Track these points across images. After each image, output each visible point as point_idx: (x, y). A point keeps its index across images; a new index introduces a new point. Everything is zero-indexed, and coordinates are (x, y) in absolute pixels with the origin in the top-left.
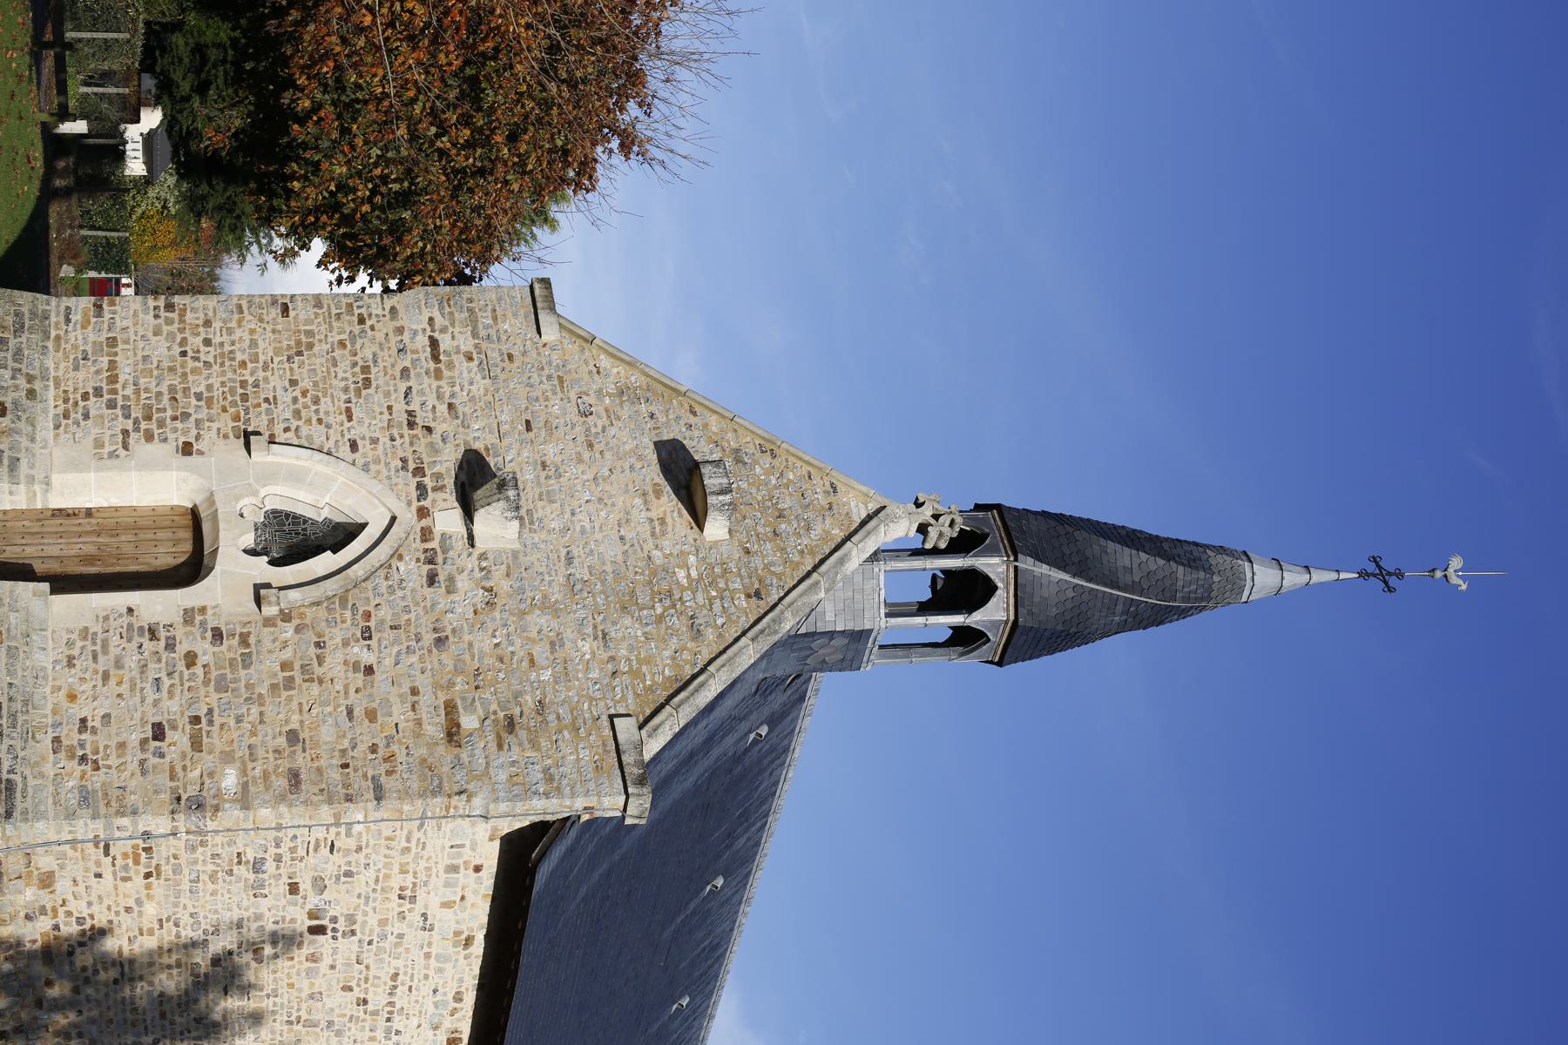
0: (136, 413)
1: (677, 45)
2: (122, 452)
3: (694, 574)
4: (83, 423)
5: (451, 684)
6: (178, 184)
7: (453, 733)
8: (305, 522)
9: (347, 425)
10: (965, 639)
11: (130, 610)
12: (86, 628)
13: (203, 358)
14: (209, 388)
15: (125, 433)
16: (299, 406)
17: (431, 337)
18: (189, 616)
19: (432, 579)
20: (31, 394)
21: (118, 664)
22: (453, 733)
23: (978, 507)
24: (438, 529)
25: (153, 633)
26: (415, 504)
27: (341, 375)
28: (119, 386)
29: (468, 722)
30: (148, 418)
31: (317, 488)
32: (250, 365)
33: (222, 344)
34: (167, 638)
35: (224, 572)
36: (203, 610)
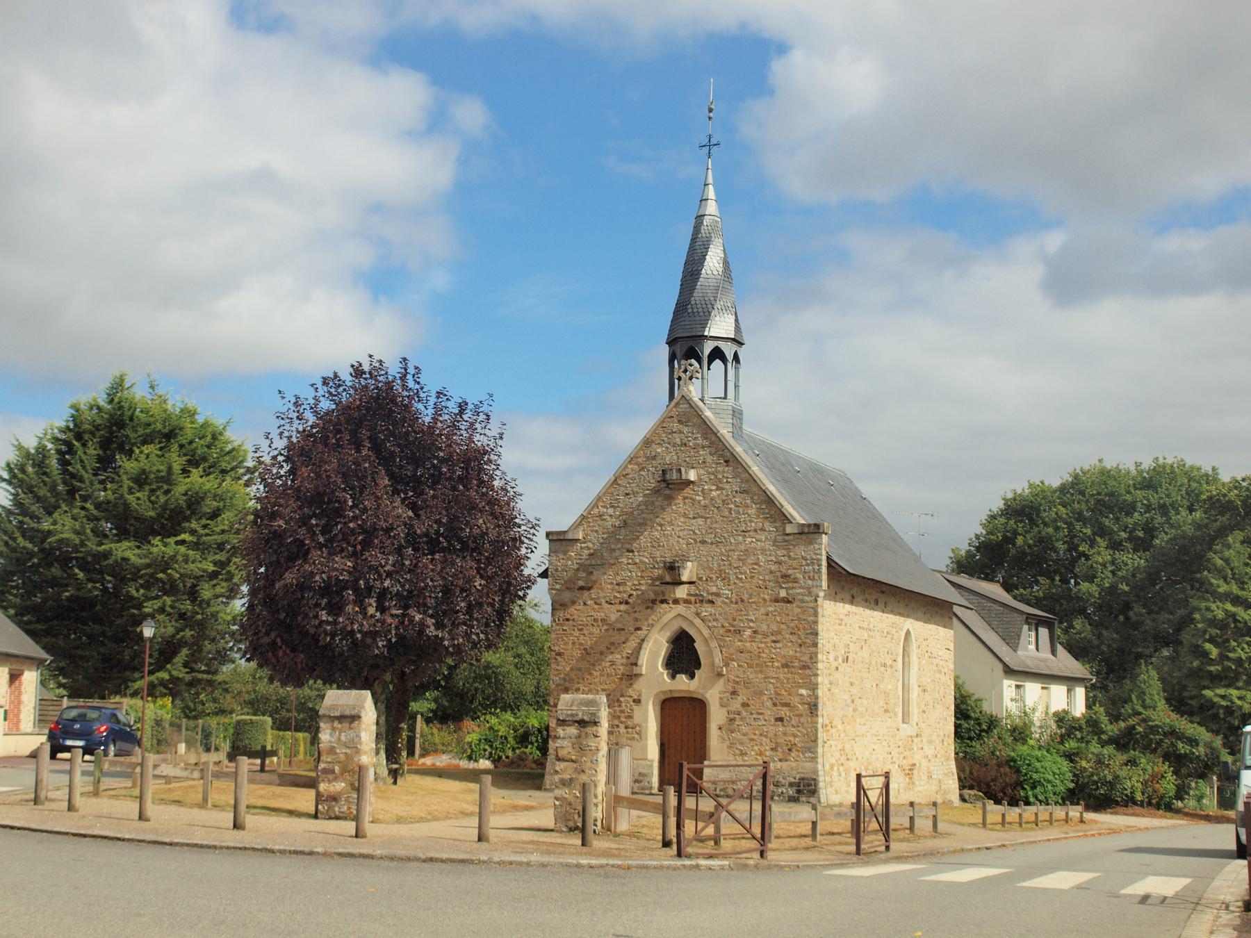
6: (174, 706)
7: (787, 601)
22: (787, 601)
23: (5, 719)
24: (685, 596)
25: (732, 720)
29: (783, 593)
31: (655, 649)
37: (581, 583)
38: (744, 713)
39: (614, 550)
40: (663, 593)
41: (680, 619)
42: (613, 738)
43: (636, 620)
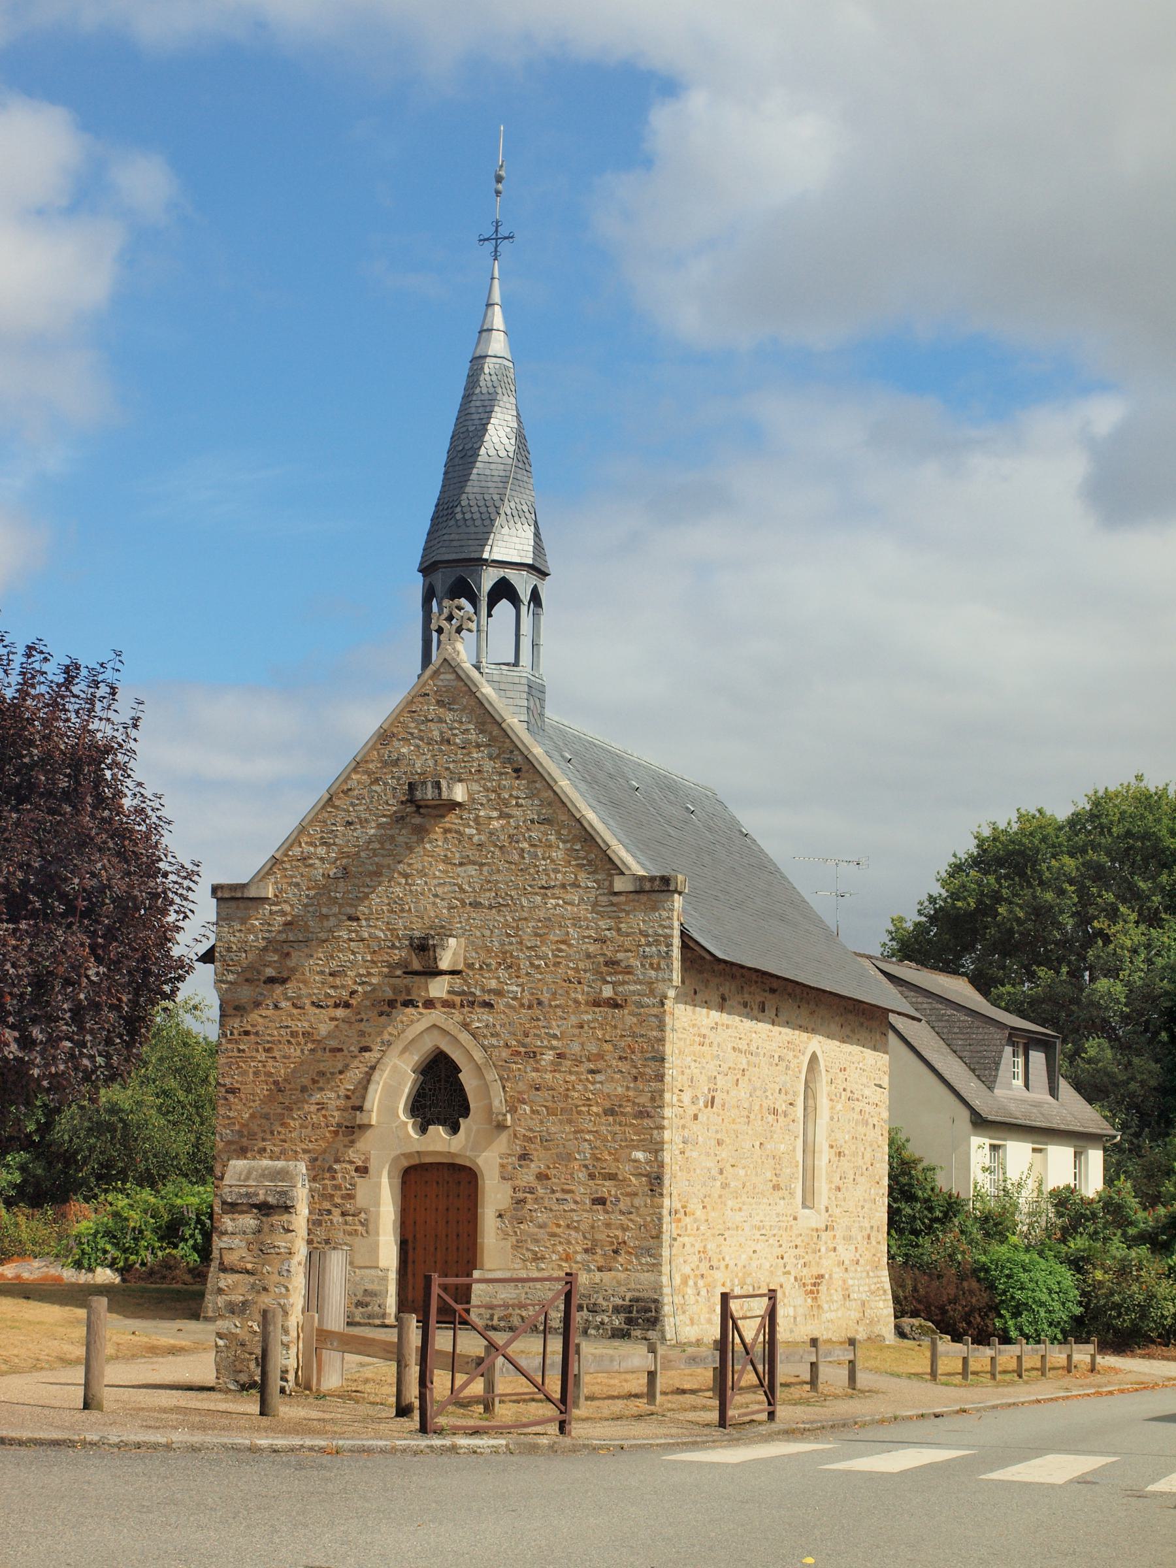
0: (327, 1205)
3: (495, 814)
9: (346, 1052)
10: (535, 597)
11: (500, 1216)
19: (488, 1005)
31: (393, 1083)
34: (524, 1192)
37: (270, 972)
38: (541, 1191)
40: (408, 991)
41: (436, 1032)
43: (362, 1034)
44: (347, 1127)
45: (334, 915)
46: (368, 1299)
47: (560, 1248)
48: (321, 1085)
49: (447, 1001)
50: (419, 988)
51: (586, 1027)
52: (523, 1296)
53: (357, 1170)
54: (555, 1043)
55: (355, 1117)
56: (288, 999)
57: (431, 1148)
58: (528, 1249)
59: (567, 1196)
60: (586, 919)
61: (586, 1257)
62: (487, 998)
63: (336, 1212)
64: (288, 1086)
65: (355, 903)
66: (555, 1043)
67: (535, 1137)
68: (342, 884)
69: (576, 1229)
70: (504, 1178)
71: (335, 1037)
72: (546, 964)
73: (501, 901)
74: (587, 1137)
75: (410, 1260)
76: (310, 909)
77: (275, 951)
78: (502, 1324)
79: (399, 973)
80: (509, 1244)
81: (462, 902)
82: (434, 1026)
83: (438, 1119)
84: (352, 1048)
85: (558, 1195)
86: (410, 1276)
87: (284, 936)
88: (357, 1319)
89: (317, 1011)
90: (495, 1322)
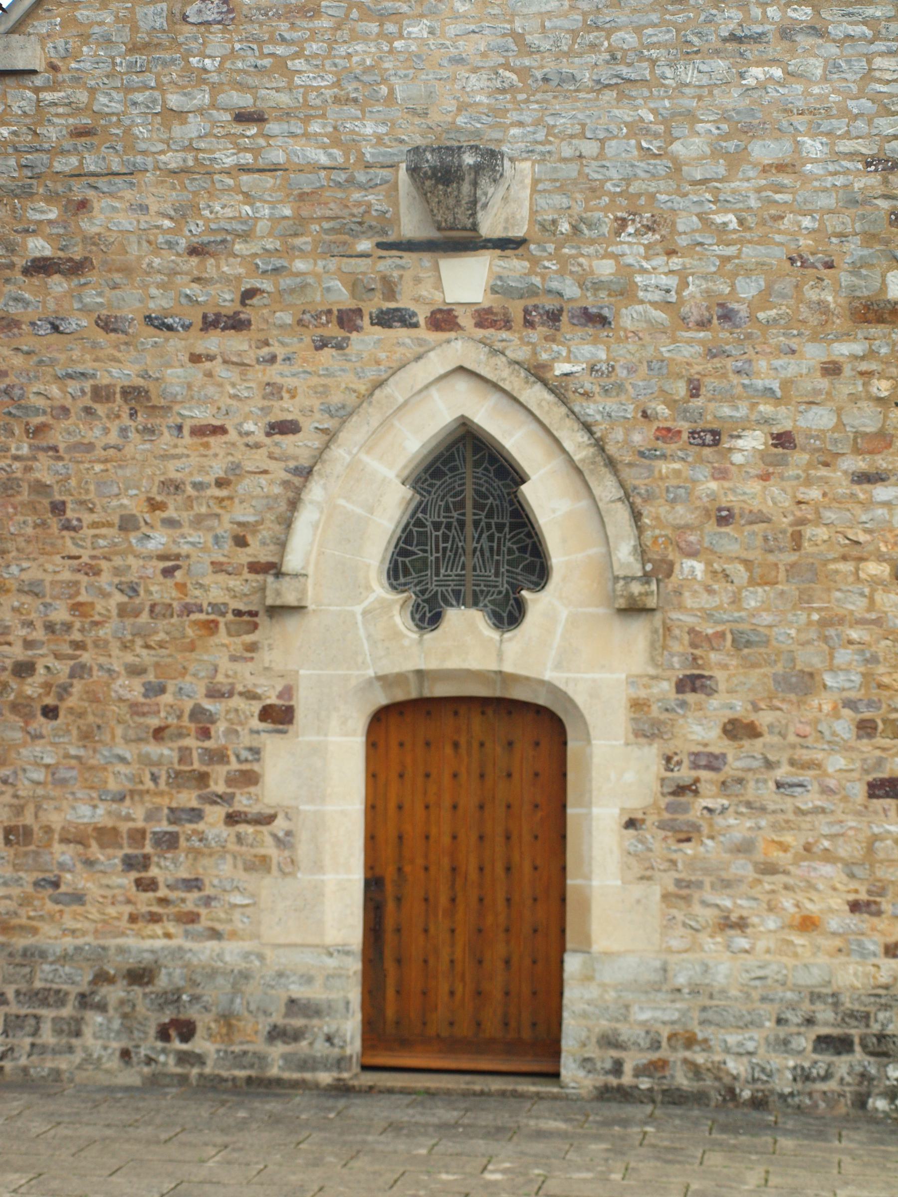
0: (188, 798)
1: (454, 102)
2: (280, 825)
4: (208, 891)
5: (822, 307)
8: (419, 523)
9: (233, 435)
11: (631, 824)
12: (665, 897)
13: (63, 678)
14: (135, 671)
15: (232, 819)
16: (185, 516)
17: (26, 272)
18: (647, 725)
19: (596, 320)
20: (140, 976)
21: (744, 848)
26: (423, 333)
27: (113, 437)
28: (124, 827)
30: (202, 779)
31: (363, 497)
32: (83, 598)
33: (29, 644)
34: (695, 766)
35: (558, 666)
36: (637, 705)
37: (38, 247)
38: (735, 765)
39: (181, 115)
40: (390, 289)
41: (462, 385)
42: (51, 1000)
43: (274, 391)
44: (238, 613)
45: (200, 111)
46: (298, 1022)
47: (787, 903)
48: (171, 513)
49: (489, 311)
50: (417, 280)
51: (847, 371)
52: (696, 1015)
53: (267, 713)
54: (765, 408)
55: (263, 589)
56: (86, 310)
57: (453, 663)
58: (705, 904)
59: (806, 776)
60: (844, 112)
61: (854, 921)
62: (591, 302)
63: (215, 814)
64: (87, 518)
65: (251, 81)
66: (765, 408)
67: (722, 635)
68: (216, 37)
69: (828, 857)
70: (639, 734)
71: (206, 401)
72: (741, 222)
73: (625, 71)
74: (854, 635)
75: (389, 923)
76: (139, 97)
77: (52, 197)
78: (645, 1084)
79: (365, 245)
80: (656, 891)
81: (523, 73)
82: (461, 369)
83: (457, 594)
84: (249, 426)
85: (783, 772)
86: (390, 965)
87: (74, 161)
88: (274, 1071)
89: (160, 337)
90: (627, 1079)
